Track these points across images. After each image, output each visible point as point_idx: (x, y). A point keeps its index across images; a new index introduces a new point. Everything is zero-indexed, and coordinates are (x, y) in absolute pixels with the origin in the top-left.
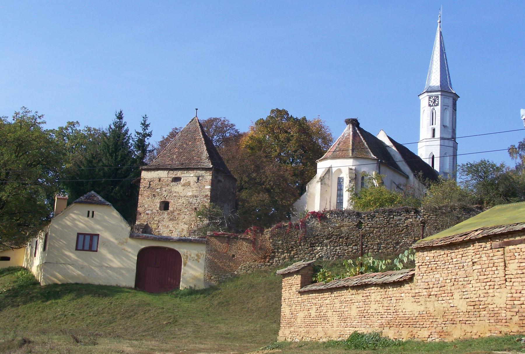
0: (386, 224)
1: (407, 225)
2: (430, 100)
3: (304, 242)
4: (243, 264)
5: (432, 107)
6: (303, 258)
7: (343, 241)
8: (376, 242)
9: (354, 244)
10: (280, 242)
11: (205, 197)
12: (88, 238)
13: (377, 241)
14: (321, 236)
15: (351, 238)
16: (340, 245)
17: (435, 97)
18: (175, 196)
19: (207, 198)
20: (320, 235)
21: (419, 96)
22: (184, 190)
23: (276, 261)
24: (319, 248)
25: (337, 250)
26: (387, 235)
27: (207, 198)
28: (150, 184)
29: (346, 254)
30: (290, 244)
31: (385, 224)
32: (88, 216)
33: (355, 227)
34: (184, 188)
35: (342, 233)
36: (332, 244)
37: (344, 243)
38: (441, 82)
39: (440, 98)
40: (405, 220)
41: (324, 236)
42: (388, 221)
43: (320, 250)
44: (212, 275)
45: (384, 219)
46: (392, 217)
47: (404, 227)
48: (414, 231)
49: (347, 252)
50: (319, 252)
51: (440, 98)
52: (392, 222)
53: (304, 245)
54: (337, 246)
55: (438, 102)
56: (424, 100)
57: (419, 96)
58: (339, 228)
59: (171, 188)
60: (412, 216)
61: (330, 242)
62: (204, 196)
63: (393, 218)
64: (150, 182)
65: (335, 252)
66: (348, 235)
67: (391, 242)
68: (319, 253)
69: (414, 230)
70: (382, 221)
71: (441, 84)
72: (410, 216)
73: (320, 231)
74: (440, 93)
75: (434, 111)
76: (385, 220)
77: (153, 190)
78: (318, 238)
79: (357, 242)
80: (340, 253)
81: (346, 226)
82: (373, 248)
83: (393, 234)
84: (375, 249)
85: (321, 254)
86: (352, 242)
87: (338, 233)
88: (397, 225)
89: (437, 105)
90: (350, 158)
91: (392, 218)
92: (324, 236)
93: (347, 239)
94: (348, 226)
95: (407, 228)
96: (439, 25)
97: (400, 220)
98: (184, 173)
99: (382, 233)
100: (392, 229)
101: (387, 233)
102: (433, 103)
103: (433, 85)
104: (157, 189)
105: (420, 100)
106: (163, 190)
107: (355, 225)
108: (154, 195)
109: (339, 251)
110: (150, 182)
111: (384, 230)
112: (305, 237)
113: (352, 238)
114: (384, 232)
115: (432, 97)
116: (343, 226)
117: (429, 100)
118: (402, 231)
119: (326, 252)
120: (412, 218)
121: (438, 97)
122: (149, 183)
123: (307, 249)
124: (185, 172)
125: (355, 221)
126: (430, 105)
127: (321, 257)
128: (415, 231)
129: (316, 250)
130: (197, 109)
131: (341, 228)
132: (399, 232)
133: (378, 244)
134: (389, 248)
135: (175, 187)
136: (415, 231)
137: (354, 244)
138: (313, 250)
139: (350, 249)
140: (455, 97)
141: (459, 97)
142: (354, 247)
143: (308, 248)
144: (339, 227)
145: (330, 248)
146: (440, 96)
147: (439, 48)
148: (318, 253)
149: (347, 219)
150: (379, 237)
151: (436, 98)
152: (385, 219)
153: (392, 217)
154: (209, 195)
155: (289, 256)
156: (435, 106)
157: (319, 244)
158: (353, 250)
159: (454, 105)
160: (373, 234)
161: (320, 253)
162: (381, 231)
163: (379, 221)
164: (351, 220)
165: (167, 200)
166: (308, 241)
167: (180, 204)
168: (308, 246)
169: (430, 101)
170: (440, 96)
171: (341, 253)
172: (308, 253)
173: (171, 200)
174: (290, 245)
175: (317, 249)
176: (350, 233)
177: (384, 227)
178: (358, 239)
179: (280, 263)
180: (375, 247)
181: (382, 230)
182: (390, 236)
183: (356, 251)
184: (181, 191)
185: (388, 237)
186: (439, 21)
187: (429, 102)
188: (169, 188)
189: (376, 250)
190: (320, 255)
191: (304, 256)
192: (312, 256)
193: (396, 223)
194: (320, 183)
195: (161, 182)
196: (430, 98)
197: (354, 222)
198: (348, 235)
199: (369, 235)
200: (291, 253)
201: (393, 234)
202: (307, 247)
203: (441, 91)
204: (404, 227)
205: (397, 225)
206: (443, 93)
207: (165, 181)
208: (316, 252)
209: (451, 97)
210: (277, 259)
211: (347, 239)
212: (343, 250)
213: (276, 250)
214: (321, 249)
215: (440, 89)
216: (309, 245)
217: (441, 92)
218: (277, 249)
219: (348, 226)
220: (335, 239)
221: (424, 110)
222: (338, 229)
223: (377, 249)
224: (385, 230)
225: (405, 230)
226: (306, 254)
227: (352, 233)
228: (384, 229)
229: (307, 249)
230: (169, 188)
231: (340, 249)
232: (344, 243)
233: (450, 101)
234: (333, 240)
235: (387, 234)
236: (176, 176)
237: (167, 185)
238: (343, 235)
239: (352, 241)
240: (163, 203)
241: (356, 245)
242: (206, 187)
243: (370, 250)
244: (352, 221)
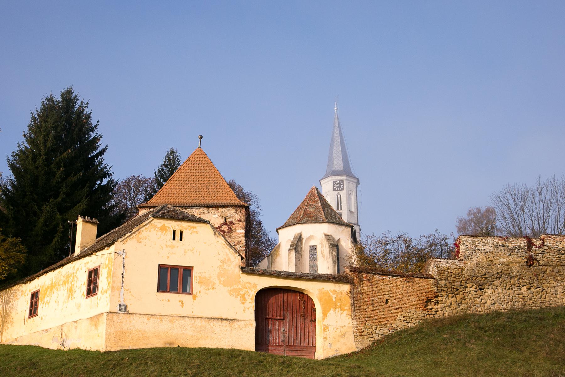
5: (337, 192)
12: (181, 272)
17: (340, 181)
27: (241, 245)
32: (174, 239)
44: (363, 329)
51: (345, 183)
55: (343, 186)
75: (339, 196)
89: (343, 189)
90: (323, 222)
121: (342, 182)
124: (206, 211)
126: (334, 190)
130: (201, 137)
143: (477, 291)
146: (345, 181)
151: (341, 183)
154: (244, 241)
156: (340, 190)
169: (343, 185)
187: (334, 187)
194: (294, 251)
196: (334, 182)
206: (348, 178)
209: (354, 182)
235: (562, 274)
242: (238, 231)
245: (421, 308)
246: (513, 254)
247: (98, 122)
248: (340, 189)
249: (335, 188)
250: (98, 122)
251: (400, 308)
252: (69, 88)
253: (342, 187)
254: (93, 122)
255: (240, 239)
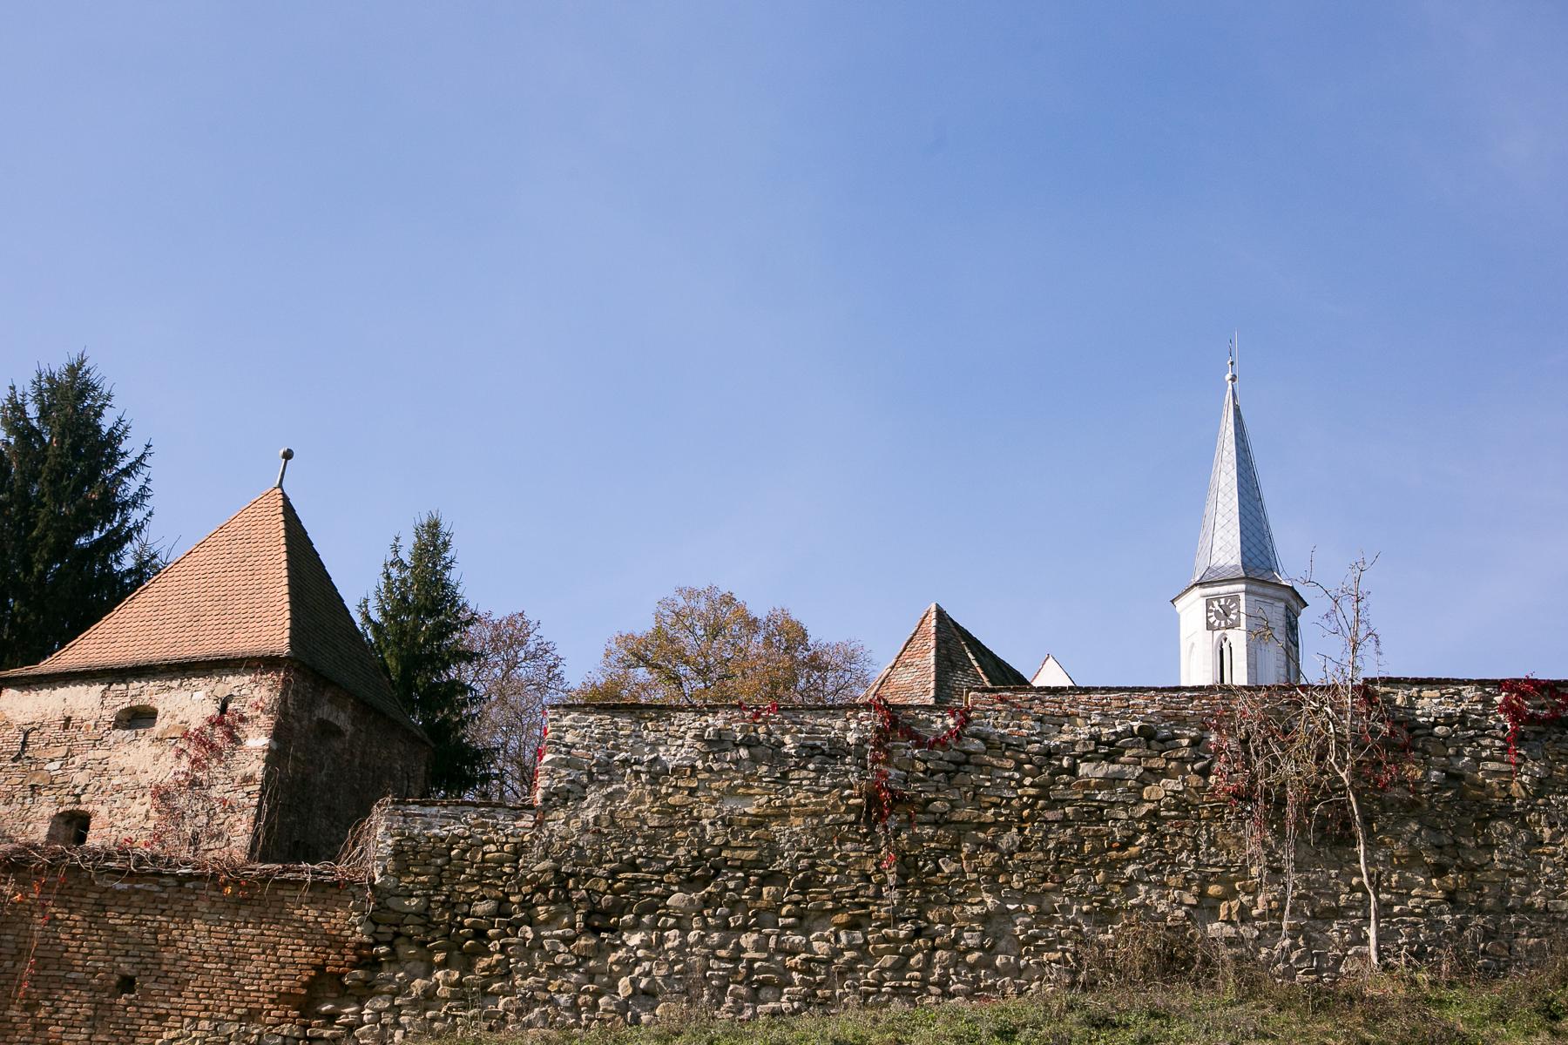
0: (1032, 806)
1: (1153, 814)
2: (1212, 611)
3: (554, 901)
4: (173, 1034)
5: (1218, 634)
6: (540, 995)
7: (777, 897)
8: (977, 909)
9: (841, 918)
10: (414, 901)
11: (240, 785)
13: (982, 902)
14: (655, 866)
15: (828, 878)
16: (760, 925)
18: (119, 789)
19: (247, 789)
20: (647, 865)
21: (1172, 601)
22: (157, 758)
23: (378, 1012)
24: (635, 939)
25: (744, 950)
26: (1040, 868)
27: (247, 789)
28: (24, 744)
29: (794, 974)
30: (467, 915)
31: (1025, 806)
33: (852, 817)
34: (159, 751)
35: (774, 851)
36: (714, 916)
37: (784, 911)
38: (1243, 553)
39: (1243, 603)
40: (1143, 782)
41: (669, 870)
42: (1044, 789)
43: (640, 953)
45: (1017, 775)
46: (1065, 763)
47: (1140, 820)
48: (1196, 848)
49: (807, 960)
50: (638, 961)
51: (1243, 603)
52: (1069, 795)
53: (550, 922)
54: (745, 928)
56: (1192, 608)
57: (1172, 601)
58: (761, 824)
59: (108, 753)
60: (1182, 760)
61: (706, 902)
62: (238, 779)
63: (1073, 770)
64: (27, 734)
65: (730, 960)
66: (813, 866)
67: (1065, 909)
68: (638, 970)
69: (1195, 839)
70: (1009, 787)
71: (1246, 560)
72: (1173, 764)
73: (651, 840)
74: (1242, 587)
75: (1225, 646)
76: (1028, 781)
77: (33, 768)
78: (637, 881)
79: (864, 906)
80: (761, 970)
81: (797, 815)
82: (959, 937)
83: (1073, 860)
84: (969, 950)
85: (647, 974)
86: (830, 905)
87: (753, 854)
88: (1097, 814)
91: (1062, 770)
92: (669, 870)
93: (803, 886)
94: (814, 814)
95: (1152, 829)
96: (1230, 387)
97: (1110, 782)
98: (170, 688)
99: (1011, 855)
100: (1069, 831)
101: (1040, 855)
102: (1220, 617)
103: (1218, 565)
104: (52, 760)
105: (1178, 616)
106: (73, 763)
107: (849, 810)
108: (32, 787)
109: (757, 955)
110: (27, 734)
111: (1018, 839)
112: (557, 871)
113: (832, 884)
114: (1021, 849)
115: (1218, 599)
116: (782, 814)
117: (1208, 611)
118: (1123, 847)
119: (676, 962)
120: (1184, 772)
122: (22, 737)
123: (567, 941)
125: (851, 787)
126: (1210, 626)
127: (645, 992)
128: (1204, 847)
129: (621, 953)
130: (288, 455)
131: (774, 827)
132: (1110, 848)
133: (986, 918)
134: (1050, 947)
135: (126, 750)
136: (1204, 847)
137: (841, 918)
138: (600, 951)
139: (821, 948)
140: (1294, 602)
141: (1306, 605)
142: (843, 936)
143: (572, 939)
144: (759, 822)
145: (702, 938)
147: (1234, 453)
148: (627, 966)
149: (804, 773)
150: (993, 878)
151: (1230, 604)
152: (1025, 774)
153: (1065, 763)
154: (259, 775)
155: (459, 983)
157: (639, 916)
158: (838, 953)
159: (1292, 628)
160: (960, 861)
161: (646, 965)
162: (1004, 843)
163: (995, 786)
164: (833, 777)
165: (82, 808)
166: (575, 896)
167: (134, 821)
168: (572, 925)
169: (1209, 614)
170: (1242, 596)
171: (768, 970)
172: (574, 968)
173: (98, 807)
174: (467, 921)
175: (624, 944)
176: (819, 856)
177: (1022, 820)
178: (871, 892)
179: (397, 1025)
180: (970, 939)
181: (1009, 838)
182: (1056, 870)
183: (856, 960)
184: (147, 763)
185: (1044, 880)
186: (1228, 376)
188: (100, 754)
189: (971, 958)
190: (643, 983)
191: (547, 984)
192: (591, 987)
193: (1086, 798)
195: (71, 732)
196: (1209, 603)
197: (847, 792)
198: (813, 866)
199: (930, 865)
200: (469, 968)
201: (1073, 860)
202: (569, 932)
203: (1246, 579)
204: (1140, 820)
205: (1097, 814)
206: (1254, 588)
207: (88, 726)
208: (617, 962)
209: (1281, 600)
210: (381, 1003)
211: (803, 886)
212: (779, 950)
213: (383, 949)
214: (646, 945)
215: (1243, 575)
216: (578, 918)
217: (1246, 583)
218: (389, 944)
219: (814, 814)
220: (731, 885)
221: (1193, 644)
222: (754, 826)
223: (981, 948)
224: (1026, 840)
225: (1143, 838)
226: (557, 970)
227: (834, 851)
228: (1021, 830)
229: (567, 941)
230: (100, 754)
231: (760, 946)
232: (784, 911)
233: (1276, 614)
234: (721, 895)
235: (1039, 862)
236: (134, 704)
237: (97, 742)
238: (781, 864)
239: (834, 899)
240: (68, 823)
241: (852, 925)
243: (938, 954)
244: (834, 786)
245: (272, 1013)
246: (795, 775)
247: (148, 446)
248: (1226, 623)
249: (1212, 620)
250: (148, 446)
251: (171, 1012)
252: (74, 358)
253: (1233, 617)
254: (131, 447)
255: (249, 771)
